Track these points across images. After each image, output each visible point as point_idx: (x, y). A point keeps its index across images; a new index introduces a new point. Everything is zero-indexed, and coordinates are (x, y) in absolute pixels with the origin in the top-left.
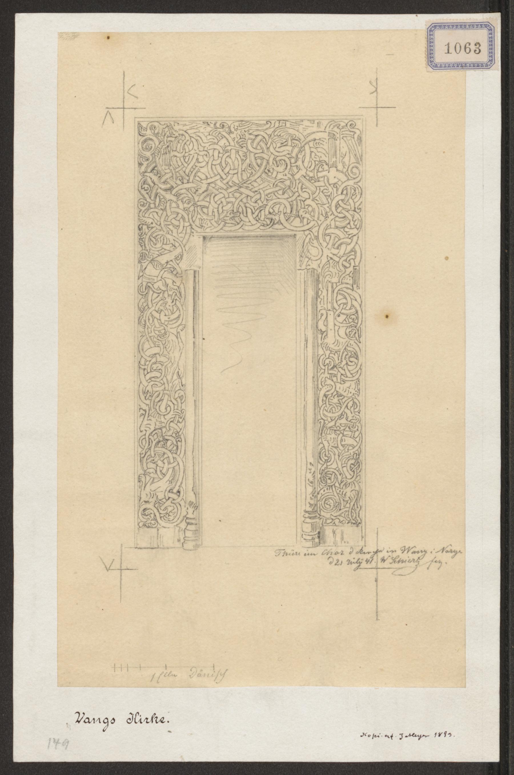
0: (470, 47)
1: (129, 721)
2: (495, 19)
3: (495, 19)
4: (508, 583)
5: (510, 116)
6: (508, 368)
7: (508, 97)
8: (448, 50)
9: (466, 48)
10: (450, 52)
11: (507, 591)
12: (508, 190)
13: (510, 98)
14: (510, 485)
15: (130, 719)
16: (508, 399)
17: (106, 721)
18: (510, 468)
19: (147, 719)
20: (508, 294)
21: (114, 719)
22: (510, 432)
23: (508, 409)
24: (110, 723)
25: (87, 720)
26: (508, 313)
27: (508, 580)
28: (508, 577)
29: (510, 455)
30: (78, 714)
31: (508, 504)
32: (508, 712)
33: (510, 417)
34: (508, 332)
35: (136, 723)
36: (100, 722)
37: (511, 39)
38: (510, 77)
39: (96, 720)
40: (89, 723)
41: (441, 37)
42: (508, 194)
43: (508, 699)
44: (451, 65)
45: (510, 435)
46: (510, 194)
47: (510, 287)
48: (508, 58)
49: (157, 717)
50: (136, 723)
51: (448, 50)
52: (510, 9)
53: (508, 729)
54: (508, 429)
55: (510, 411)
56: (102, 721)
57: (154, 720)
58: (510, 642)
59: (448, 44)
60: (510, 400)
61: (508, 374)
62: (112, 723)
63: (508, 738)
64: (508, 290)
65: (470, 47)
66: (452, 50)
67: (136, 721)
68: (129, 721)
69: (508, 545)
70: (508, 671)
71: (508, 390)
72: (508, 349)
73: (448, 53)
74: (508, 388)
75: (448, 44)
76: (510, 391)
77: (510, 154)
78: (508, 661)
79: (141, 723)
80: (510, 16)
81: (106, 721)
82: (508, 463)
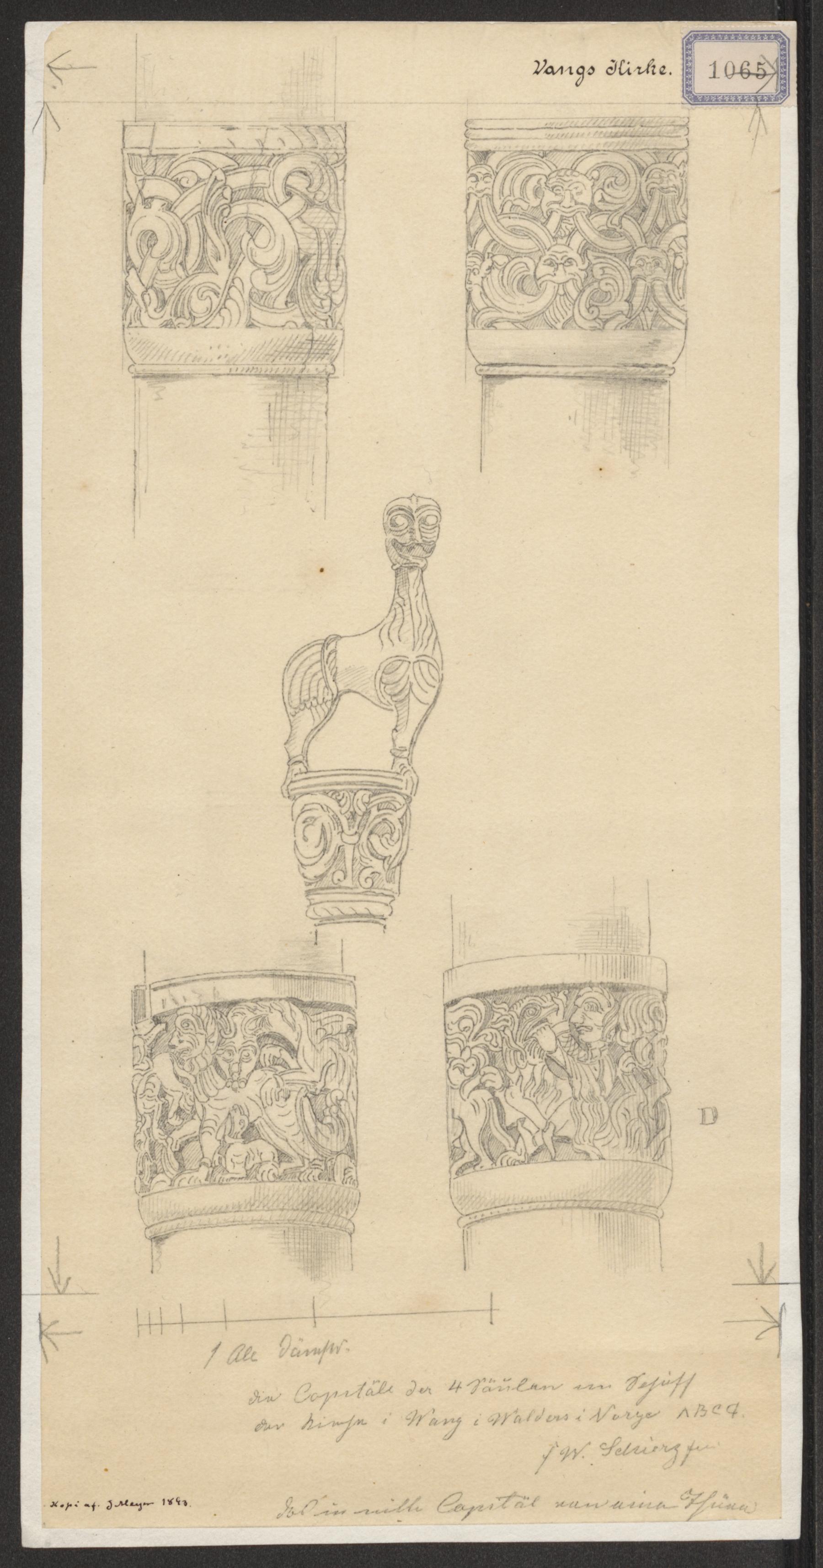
0: (748, 68)
1: (610, 71)
2: (789, 28)
3: (789, 28)
4: (812, 1134)
5: (813, 388)
6: (811, 792)
7: (810, 359)
8: (714, 73)
9: (744, 73)
10: (717, 75)
11: (810, 1146)
12: (811, 507)
13: (814, 361)
14: (815, 977)
15: (611, 68)
16: (812, 842)
17: (581, 70)
18: (815, 950)
19: (639, 68)
20: (811, 672)
21: (592, 68)
22: (815, 894)
23: (812, 858)
24: (586, 74)
25: (550, 70)
26: (811, 703)
27: (812, 1130)
28: (812, 1124)
29: (815, 930)
30: (536, 64)
31: (812, 1009)
32: (813, 1340)
33: (814, 870)
34: (812, 735)
35: (653, 74)
36: (571, 73)
37: (815, 266)
38: (813, 327)
39: (564, 69)
40: (554, 74)
41: (704, 52)
42: (810, 513)
43: (813, 1320)
44: (746, 37)
45: (814, 898)
46: (814, 514)
47: (814, 661)
48: (810, 297)
49: (654, 66)
50: (621, 74)
51: (714, 73)
52: (813, 218)
53: (813, 1367)
54: (812, 889)
55: (815, 860)
56: (574, 71)
57: (650, 69)
58: (815, 1228)
59: (715, 63)
60: (814, 842)
61: (811, 801)
62: (590, 74)
63: (813, 1381)
64: (811, 668)
65: (748, 68)
66: (720, 73)
67: (623, 72)
68: (610, 71)
69: (812, 1073)
70: (812, 1275)
71: (812, 827)
72: (811, 761)
73: (714, 77)
74: (811, 823)
75: (715, 63)
76: (815, 828)
77: (813, 451)
78: (813, 1259)
79: (629, 74)
80: (813, 229)
81: (581, 70)
82: (812, 941)
